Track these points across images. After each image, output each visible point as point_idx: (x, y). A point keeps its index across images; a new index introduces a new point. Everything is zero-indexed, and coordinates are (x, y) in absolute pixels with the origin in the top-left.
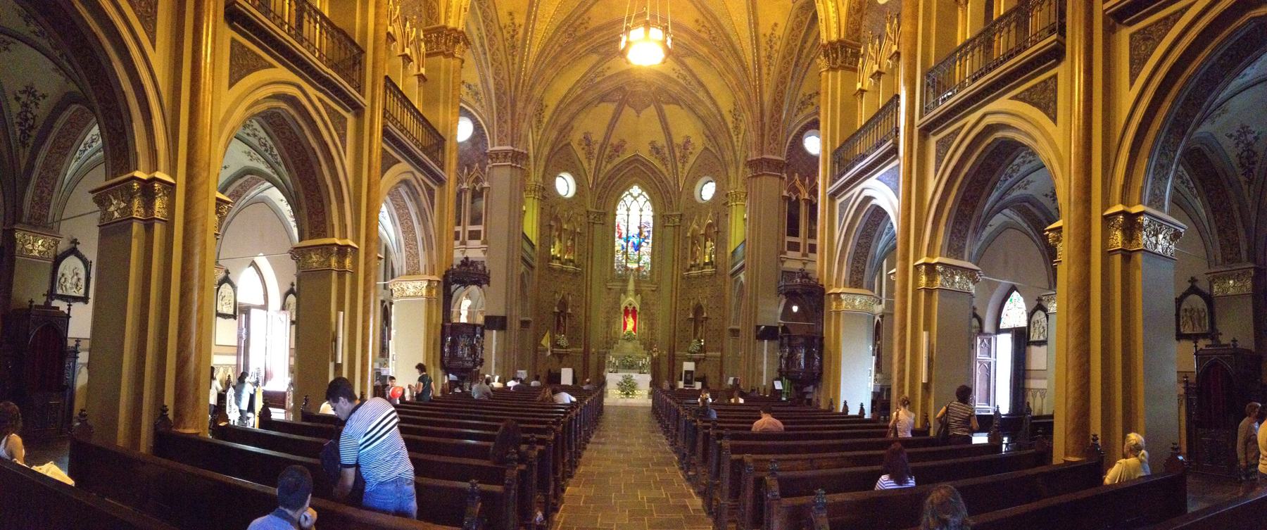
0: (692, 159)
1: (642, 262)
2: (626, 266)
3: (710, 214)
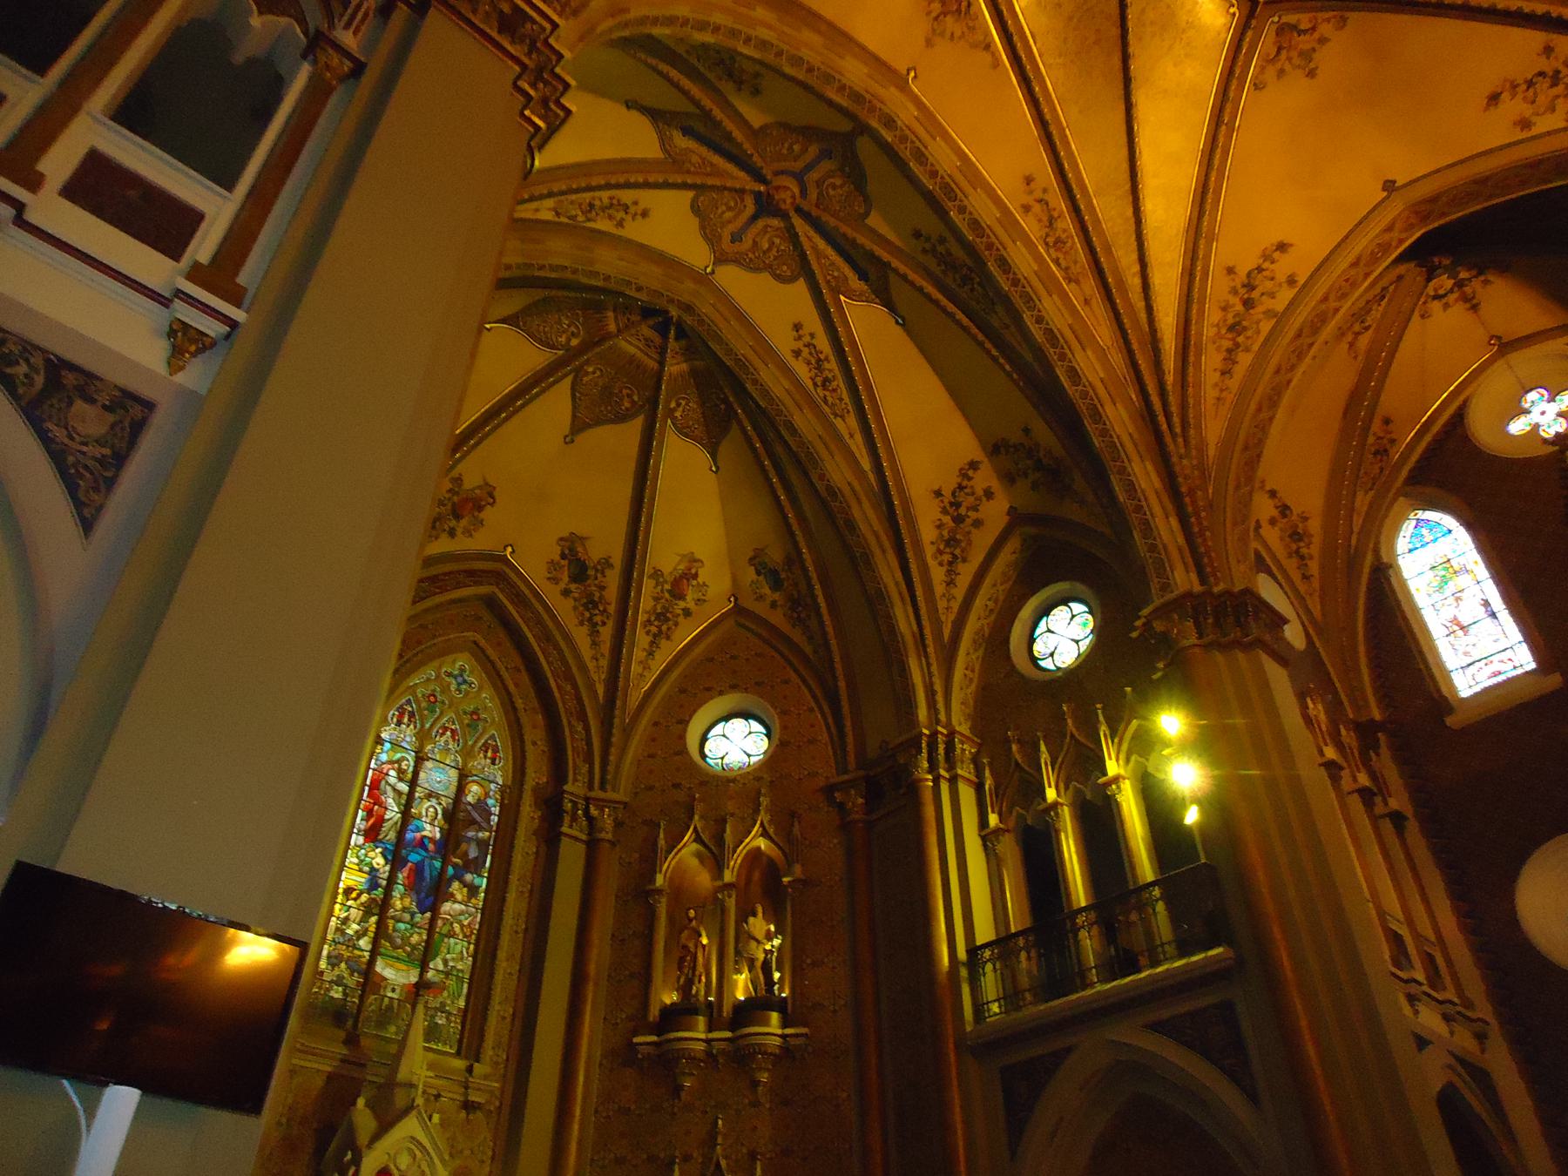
0: (686, 634)
1: (437, 963)
2: (368, 971)
3: (763, 816)
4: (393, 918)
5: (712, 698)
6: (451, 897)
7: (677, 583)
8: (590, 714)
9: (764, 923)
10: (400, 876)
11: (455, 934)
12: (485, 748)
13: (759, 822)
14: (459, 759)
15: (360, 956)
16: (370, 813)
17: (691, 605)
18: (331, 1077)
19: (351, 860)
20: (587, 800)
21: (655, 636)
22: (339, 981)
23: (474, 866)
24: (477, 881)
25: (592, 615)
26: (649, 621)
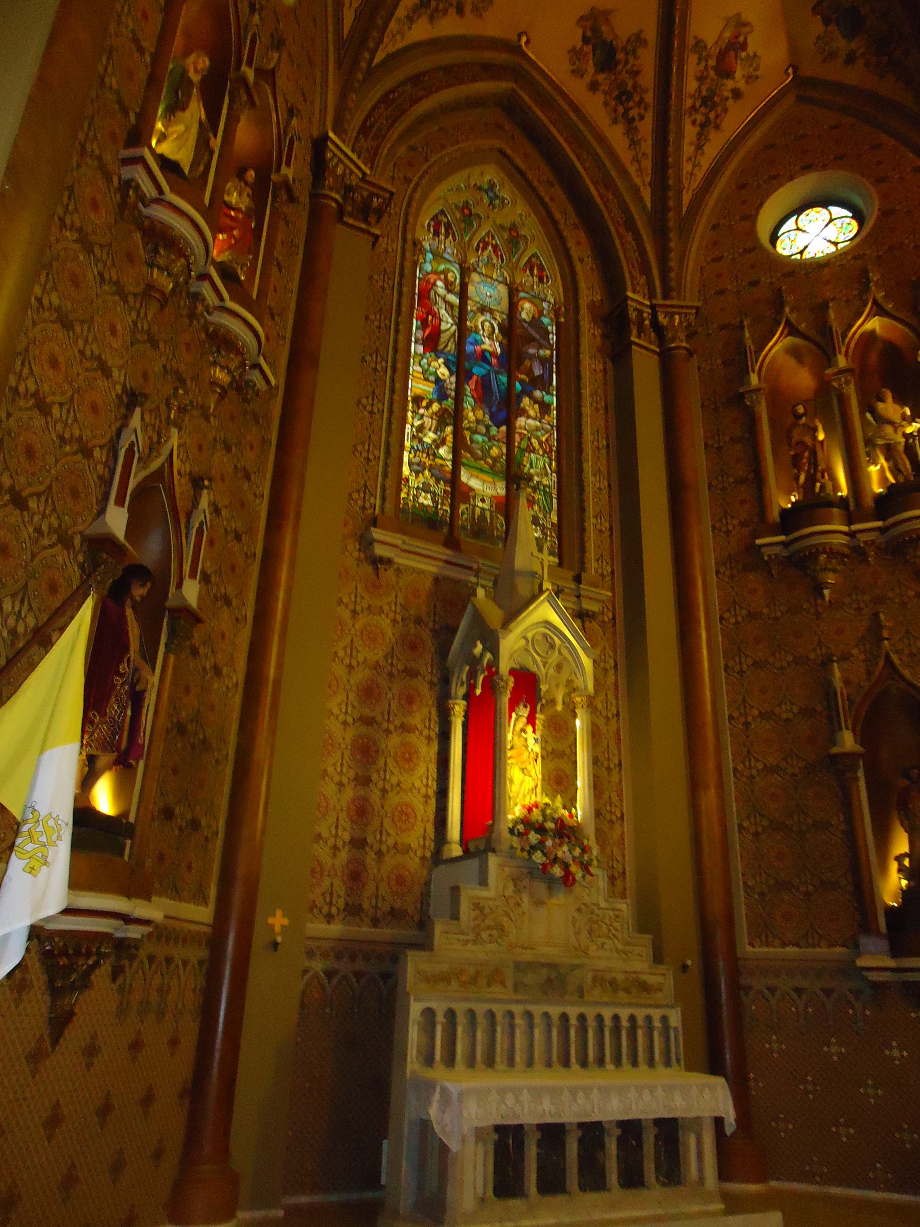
2: (454, 480)
4: (468, 429)
5: (781, 185)
6: (523, 412)
7: (722, 56)
8: (639, 224)
9: (897, 407)
10: (467, 387)
11: (534, 448)
12: (530, 265)
13: (871, 300)
14: (506, 274)
15: (442, 465)
16: (424, 324)
17: (741, 85)
18: (437, 580)
19: (415, 369)
20: (653, 307)
21: (703, 125)
22: (426, 488)
23: (542, 383)
24: (547, 398)
25: (627, 110)
26: (693, 107)
